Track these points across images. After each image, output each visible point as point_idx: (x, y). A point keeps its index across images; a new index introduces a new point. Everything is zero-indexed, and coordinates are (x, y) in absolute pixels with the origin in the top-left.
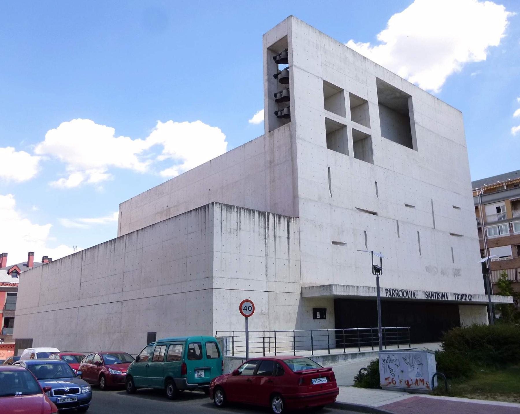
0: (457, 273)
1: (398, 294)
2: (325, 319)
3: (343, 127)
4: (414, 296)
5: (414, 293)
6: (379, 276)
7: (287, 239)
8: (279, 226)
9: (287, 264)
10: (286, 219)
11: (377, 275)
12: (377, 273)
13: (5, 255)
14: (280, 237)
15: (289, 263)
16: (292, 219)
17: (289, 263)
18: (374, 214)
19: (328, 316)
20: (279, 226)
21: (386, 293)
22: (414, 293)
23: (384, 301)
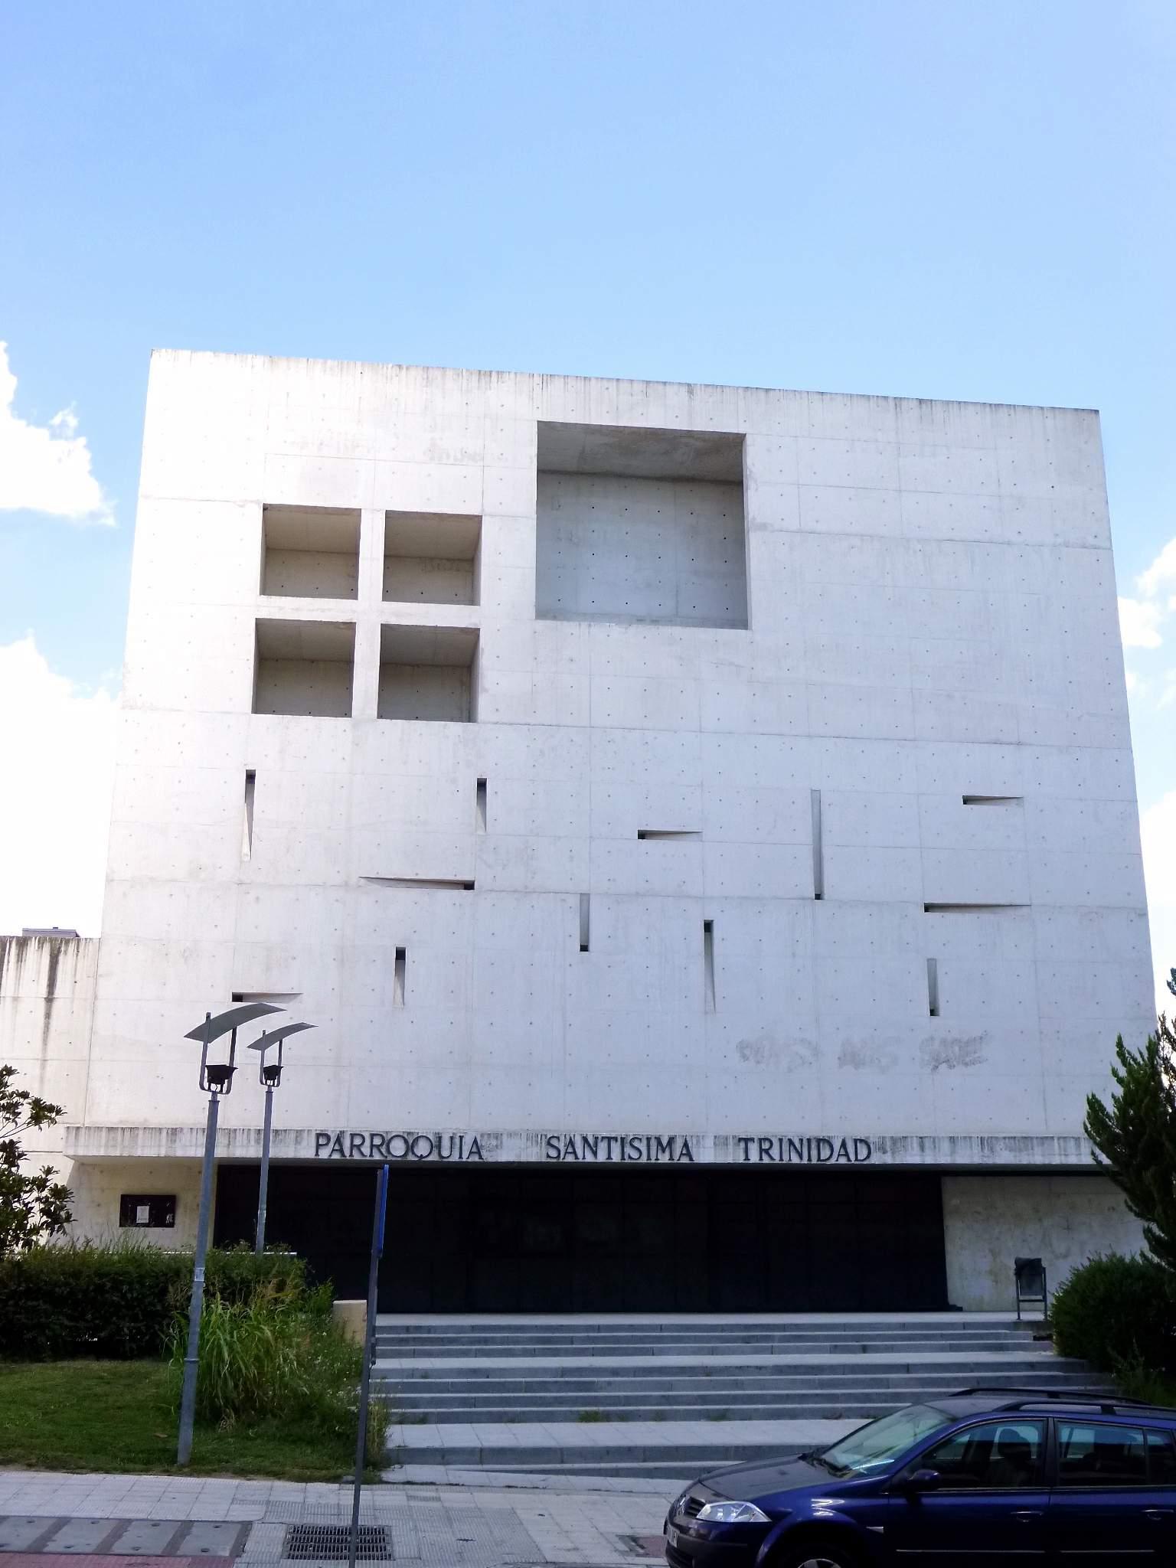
0: (959, 1054)
1: (437, 1144)
2: (172, 1225)
3: (390, 634)
4: (689, 1155)
5: (686, 1145)
6: (219, 1097)
7: (42, 1004)
8: (19, 969)
9: (38, 1071)
10: (47, 948)
11: (214, 1093)
12: (213, 1087)
13: (9, 1071)
14: (16, 999)
15: (43, 1067)
16: (72, 946)
17: (43, 1067)
18: (469, 886)
19: (181, 1217)
20: (19, 969)
21: (318, 1146)
22: (686, 1145)
23: (287, 1173)
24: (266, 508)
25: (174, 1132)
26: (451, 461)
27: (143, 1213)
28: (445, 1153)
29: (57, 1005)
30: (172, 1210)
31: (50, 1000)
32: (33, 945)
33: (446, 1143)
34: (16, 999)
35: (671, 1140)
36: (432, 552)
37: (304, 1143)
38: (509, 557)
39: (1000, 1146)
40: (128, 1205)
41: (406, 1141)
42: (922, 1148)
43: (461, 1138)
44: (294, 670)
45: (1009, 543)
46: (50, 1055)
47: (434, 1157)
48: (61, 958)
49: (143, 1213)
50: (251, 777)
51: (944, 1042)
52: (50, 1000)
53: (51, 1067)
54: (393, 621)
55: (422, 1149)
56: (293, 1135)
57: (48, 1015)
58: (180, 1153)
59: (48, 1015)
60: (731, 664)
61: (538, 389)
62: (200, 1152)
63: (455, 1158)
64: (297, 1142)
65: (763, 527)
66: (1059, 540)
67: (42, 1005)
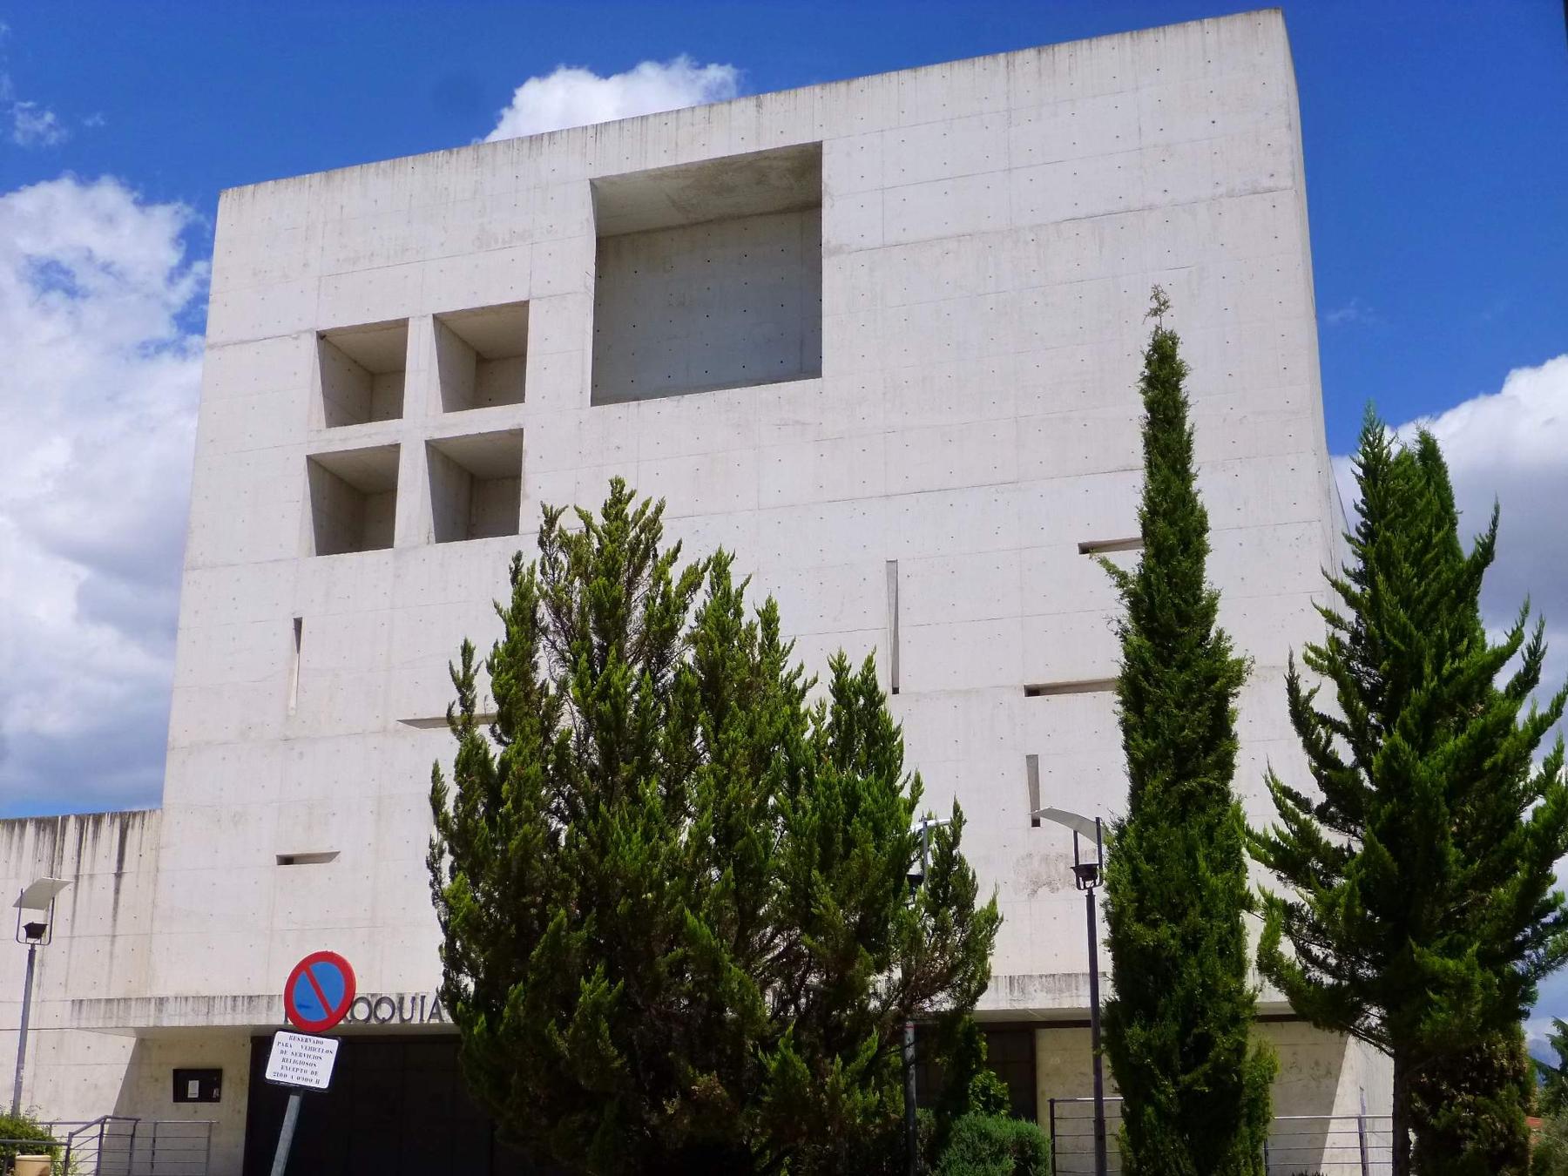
2: (218, 1100)
9: (108, 948)
16: (138, 819)
24: (322, 336)
25: (210, 1000)
26: (500, 245)
27: (193, 1088)
28: (407, 1016)
29: (125, 880)
30: (219, 1085)
31: (119, 875)
32: (106, 821)
33: (408, 1004)
34: (91, 876)
35: (402, 1000)
36: (487, 357)
37: (275, 1009)
38: (560, 349)
39: (170, 1007)
40: (181, 1078)
41: (369, 1004)
42: (234, 1008)
43: (423, 998)
44: (352, 509)
45: (1151, 208)
46: (119, 931)
47: (396, 1020)
48: (129, 832)
49: (193, 1088)
50: (298, 623)
51: (1045, 859)
52: (119, 875)
53: (120, 941)
54: (437, 436)
55: (384, 1012)
56: (264, 1002)
57: (117, 891)
58: (165, 1024)
59: (117, 891)
60: (797, 422)
61: (591, 142)
62: (1085, 1002)
63: (416, 1021)
64: (269, 1007)
65: (838, 250)
66: (1222, 190)
67: (112, 880)
